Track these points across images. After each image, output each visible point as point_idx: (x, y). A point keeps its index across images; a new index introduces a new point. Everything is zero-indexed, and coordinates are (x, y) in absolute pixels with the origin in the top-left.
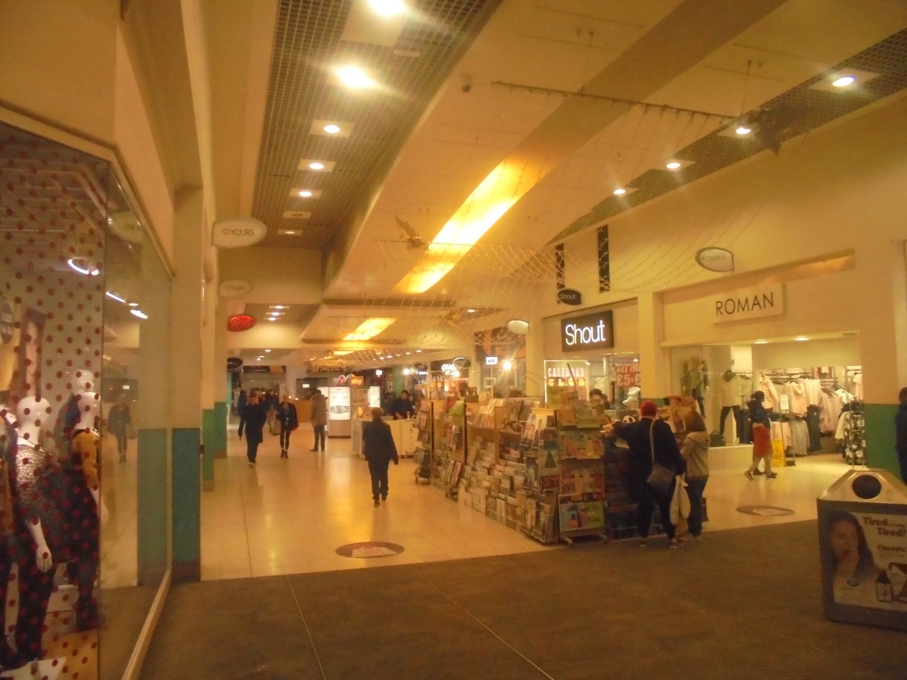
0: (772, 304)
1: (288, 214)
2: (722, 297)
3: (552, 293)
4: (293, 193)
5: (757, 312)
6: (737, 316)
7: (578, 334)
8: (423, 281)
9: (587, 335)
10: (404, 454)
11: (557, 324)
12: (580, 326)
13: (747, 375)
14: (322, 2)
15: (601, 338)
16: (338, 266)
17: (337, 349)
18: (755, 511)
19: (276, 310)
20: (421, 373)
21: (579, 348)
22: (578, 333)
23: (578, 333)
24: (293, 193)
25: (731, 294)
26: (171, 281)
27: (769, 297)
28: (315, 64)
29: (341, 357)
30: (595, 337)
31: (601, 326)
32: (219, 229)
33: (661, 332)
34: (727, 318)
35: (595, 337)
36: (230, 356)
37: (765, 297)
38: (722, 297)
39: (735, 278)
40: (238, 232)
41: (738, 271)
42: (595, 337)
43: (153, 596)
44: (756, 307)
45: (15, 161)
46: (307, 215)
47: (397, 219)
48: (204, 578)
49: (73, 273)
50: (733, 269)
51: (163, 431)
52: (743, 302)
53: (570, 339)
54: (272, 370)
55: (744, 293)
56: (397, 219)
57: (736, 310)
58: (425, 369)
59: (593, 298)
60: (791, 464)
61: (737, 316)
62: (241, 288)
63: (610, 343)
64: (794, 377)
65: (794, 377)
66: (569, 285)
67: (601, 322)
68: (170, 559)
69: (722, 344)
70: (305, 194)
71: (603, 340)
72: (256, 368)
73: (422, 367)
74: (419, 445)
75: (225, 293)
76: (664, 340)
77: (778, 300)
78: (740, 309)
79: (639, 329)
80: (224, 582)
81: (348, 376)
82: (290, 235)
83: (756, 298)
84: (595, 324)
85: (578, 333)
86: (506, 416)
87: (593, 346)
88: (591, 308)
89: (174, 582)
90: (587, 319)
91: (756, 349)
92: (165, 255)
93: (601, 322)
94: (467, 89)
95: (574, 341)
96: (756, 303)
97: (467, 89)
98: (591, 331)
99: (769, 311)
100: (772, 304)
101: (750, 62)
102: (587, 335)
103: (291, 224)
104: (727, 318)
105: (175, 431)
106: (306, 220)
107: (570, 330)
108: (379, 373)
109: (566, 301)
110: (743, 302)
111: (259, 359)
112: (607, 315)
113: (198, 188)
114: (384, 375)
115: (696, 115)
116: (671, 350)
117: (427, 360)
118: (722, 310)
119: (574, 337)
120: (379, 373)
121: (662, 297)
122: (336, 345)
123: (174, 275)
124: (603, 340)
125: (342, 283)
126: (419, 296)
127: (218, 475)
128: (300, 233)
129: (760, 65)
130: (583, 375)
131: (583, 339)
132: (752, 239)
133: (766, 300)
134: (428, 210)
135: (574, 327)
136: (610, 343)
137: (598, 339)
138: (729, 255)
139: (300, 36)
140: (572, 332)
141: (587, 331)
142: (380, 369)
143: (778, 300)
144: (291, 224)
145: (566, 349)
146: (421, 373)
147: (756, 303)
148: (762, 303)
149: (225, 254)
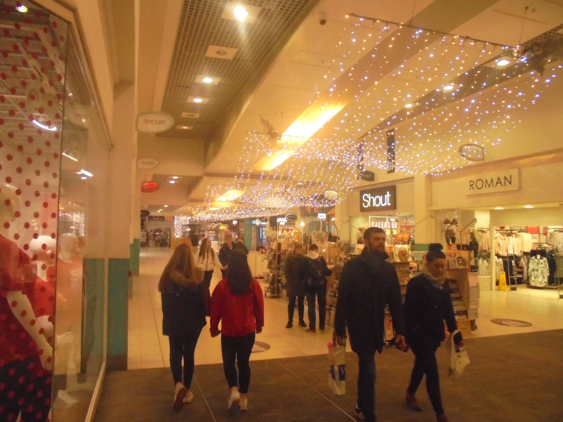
0: (510, 183)
1: (184, 115)
2: (474, 177)
4: (189, 100)
5: (499, 188)
6: (484, 190)
7: (371, 200)
8: (272, 162)
9: (378, 201)
10: (257, 276)
11: (357, 194)
12: (373, 195)
13: (485, 230)
15: (388, 203)
16: (216, 153)
17: (211, 206)
18: (504, 322)
19: (174, 180)
20: (263, 223)
21: (372, 209)
24: (189, 100)
25: (480, 176)
26: (110, 150)
27: (509, 179)
29: (214, 212)
30: (383, 202)
31: (388, 195)
32: (141, 118)
33: (430, 202)
34: (476, 191)
35: (383, 202)
36: (142, 209)
37: (505, 178)
38: (474, 177)
39: (482, 165)
40: (154, 122)
41: (486, 161)
43: (95, 383)
44: (499, 185)
46: (197, 116)
47: (261, 118)
48: (130, 367)
49: (40, 131)
50: (483, 159)
51: (103, 260)
52: (489, 182)
53: (366, 204)
54: (166, 219)
55: (492, 175)
56: (261, 118)
57: (484, 186)
58: (266, 221)
59: (382, 178)
60: (514, 289)
61: (484, 190)
62: (152, 163)
63: (394, 206)
64: (513, 232)
65: (513, 232)
67: (388, 192)
68: (105, 354)
69: (470, 209)
70: (198, 100)
71: (389, 204)
72: (156, 217)
73: (264, 219)
74: (268, 271)
75: (141, 166)
76: (432, 206)
77: (515, 181)
78: (487, 186)
79: (414, 199)
80: (144, 371)
81: (217, 224)
82: (185, 130)
83: (499, 178)
84: (383, 194)
85: (372, 199)
86: (336, 254)
87: (381, 209)
88: (381, 183)
89: (108, 370)
90: (379, 191)
91: (493, 213)
92: (107, 128)
93: (388, 192)
94: (323, 22)
95: (369, 205)
96: (499, 181)
97: (323, 22)
98: (381, 199)
99: (508, 187)
100: (510, 183)
101: (527, 8)
102: (378, 201)
103: (186, 122)
104: (476, 191)
105: (110, 260)
106: (196, 119)
107: (366, 198)
108: (235, 222)
109: (364, 178)
110: (489, 182)
111: (159, 211)
113: (131, 83)
114: (238, 224)
116: (437, 212)
117: (268, 215)
118: (474, 186)
119: (369, 203)
120: (235, 222)
121: (430, 178)
122: (209, 204)
123: (112, 146)
124: (389, 204)
125: (219, 163)
127: (135, 288)
128: (191, 128)
129: (534, 10)
130: (396, 227)
131: (374, 204)
132: (498, 138)
133: (500, 179)
134: (282, 113)
135: (369, 196)
136: (394, 206)
137: (385, 204)
138: (481, 149)
140: (368, 199)
142: (236, 220)
143: (515, 181)
144: (186, 122)
145: (362, 210)
146: (263, 223)
147: (499, 181)
148: (503, 182)
149: (143, 137)
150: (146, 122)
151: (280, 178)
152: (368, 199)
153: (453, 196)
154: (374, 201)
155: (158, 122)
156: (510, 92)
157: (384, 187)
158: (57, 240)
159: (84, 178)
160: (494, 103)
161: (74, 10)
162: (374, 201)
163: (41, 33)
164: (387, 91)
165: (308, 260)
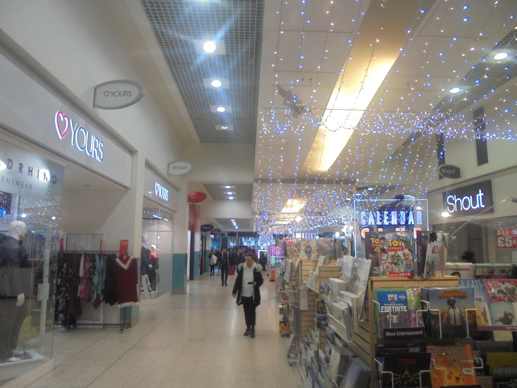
3: (434, 167)
4: (230, 110)
9: (466, 203)
17: (278, 220)
22: (458, 202)
23: (458, 202)
28: (195, 42)
35: (474, 204)
42: (474, 205)
45: (216, 270)
59: (471, 171)
66: (449, 161)
85: (458, 202)
93: (480, 191)
98: (470, 200)
102: (466, 203)
107: (451, 200)
112: (485, 185)
115: (97, 103)
126: (324, 174)
135: (454, 198)
137: (478, 206)
139: (174, 48)
141: (466, 200)
150: (107, 94)
151: (340, 180)
152: (454, 202)
154: (462, 203)
155: (122, 94)
156: (349, 151)
157: (474, 185)
159: (102, 146)
160: (496, 109)
162: (462, 203)
164: (281, 158)
165: (169, 220)
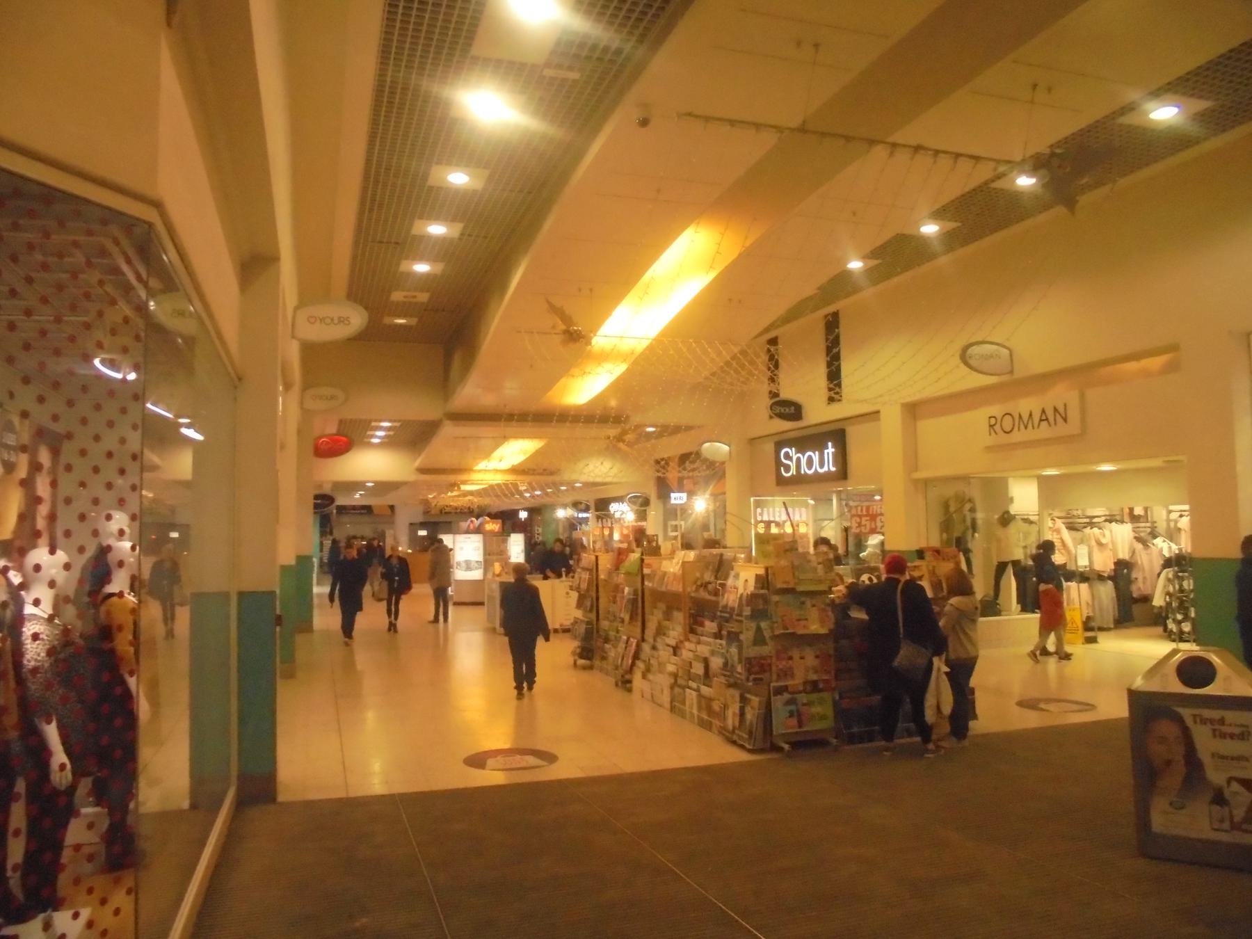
0: (1065, 420)
1: (397, 296)
2: (996, 410)
3: (762, 404)
4: (404, 266)
5: (1044, 431)
6: (1017, 436)
7: (797, 461)
8: (583, 388)
9: (810, 462)
10: (557, 626)
11: (769, 447)
12: (801, 450)
13: (1032, 518)
14: (445, 3)
15: (830, 467)
16: (467, 368)
17: (465, 482)
18: (1042, 706)
19: (381, 428)
20: (581, 515)
21: (800, 481)
22: (798, 459)
23: (798, 460)
24: (404, 266)
25: (1009, 407)
26: (236, 387)
27: (1061, 410)
28: (435, 88)
29: (471, 493)
30: (822, 465)
31: (830, 450)
32: (302, 316)
33: (912, 459)
34: (1003, 439)
35: (822, 465)
36: (317, 492)
37: (1056, 410)
38: (996, 410)
39: (1015, 384)
40: (328, 321)
41: (1018, 374)
42: (822, 465)
43: (212, 824)
44: (1044, 424)
45: (21, 222)
46: (423, 297)
47: (548, 302)
48: (281, 798)
50: (1011, 372)
51: (226, 596)
52: (1025, 417)
53: (787, 468)
54: (375, 512)
55: (1028, 405)
56: (548, 302)
57: (1016, 428)
58: (587, 510)
59: (818, 412)
60: (1092, 640)
61: (1017, 436)
62: (332, 397)
63: (843, 473)
64: (1095, 520)
65: (1095, 520)
66: (785, 394)
67: (830, 444)
68: (234, 772)
69: (997, 475)
70: (422, 268)
71: (833, 469)
72: (354, 508)
73: (583, 506)
74: (579, 614)
75: (310, 404)
76: (916, 469)
77: (1074, 415)
78: (1022, 427)
79: (882, 454)
80: (309, 804)
81: (481, 519)
82: (401, 325)
83: (1043, 411)
84: (821, 447)
85: (798, 460)
86: (698, 575)
87: (819, 478)
88: (816, 425)
89: (241, 804)
90: (811, 441)
91: (1044, 482)
92: (227, 352)
93: (830, 444)
94: (644, 123)
95: (793, 471)
96: (1044, 418)
97: (644, 123)
98: (816, 457)
99: (1062, 429)
100: (1065, 420)
101: (1035, 86)
102: (810, 462)
103: (402, 309)
104: (1003, 439)
105: (241, 595)
106: (423, 303)
107: (787, 456)
108: (523, 515)
109: (782, 416)
110: (1025, 417)
111: (357, 496)
112: (837, 435)
113: (274, 259)
114: (530, 518)
115: (961, 159)
116: (926, 483)
117: (590, 498)
118: (997, 427)
119: (793, 466)
120: (523, 515)
121: (913, 411)
122: (464, 477)
123: (240, 379)
124: (833, 469)
125: (472, 391)
126: (579, 408)
127: (301, 656)
128: (413, 321)
129: (1049, 90)
130: (804, 518)
131: (804, 469)
132: (1038, 330)
134: (591, 290)
135: (792, 452)
136: (843, 473)
137: (826, 468)
138: (1006, 352)
139: (415, 50)
140: (790, 459)
141: (810, 457)
142: (525, 509)
143: (1074, 415)
144: (402, 309)
145: (781, 482)
146: (581, 515)
147: (1044, 418)
148: (1051, 419)
149: (310, 351)
153: (957, 444)
158: (137, 900)
161: (158, 205)
163: (109, 245)
